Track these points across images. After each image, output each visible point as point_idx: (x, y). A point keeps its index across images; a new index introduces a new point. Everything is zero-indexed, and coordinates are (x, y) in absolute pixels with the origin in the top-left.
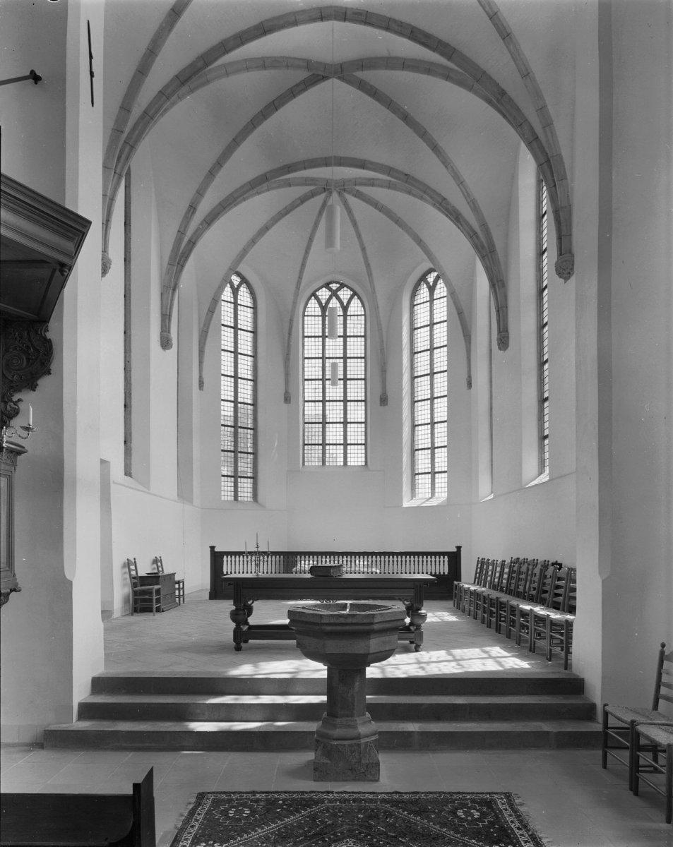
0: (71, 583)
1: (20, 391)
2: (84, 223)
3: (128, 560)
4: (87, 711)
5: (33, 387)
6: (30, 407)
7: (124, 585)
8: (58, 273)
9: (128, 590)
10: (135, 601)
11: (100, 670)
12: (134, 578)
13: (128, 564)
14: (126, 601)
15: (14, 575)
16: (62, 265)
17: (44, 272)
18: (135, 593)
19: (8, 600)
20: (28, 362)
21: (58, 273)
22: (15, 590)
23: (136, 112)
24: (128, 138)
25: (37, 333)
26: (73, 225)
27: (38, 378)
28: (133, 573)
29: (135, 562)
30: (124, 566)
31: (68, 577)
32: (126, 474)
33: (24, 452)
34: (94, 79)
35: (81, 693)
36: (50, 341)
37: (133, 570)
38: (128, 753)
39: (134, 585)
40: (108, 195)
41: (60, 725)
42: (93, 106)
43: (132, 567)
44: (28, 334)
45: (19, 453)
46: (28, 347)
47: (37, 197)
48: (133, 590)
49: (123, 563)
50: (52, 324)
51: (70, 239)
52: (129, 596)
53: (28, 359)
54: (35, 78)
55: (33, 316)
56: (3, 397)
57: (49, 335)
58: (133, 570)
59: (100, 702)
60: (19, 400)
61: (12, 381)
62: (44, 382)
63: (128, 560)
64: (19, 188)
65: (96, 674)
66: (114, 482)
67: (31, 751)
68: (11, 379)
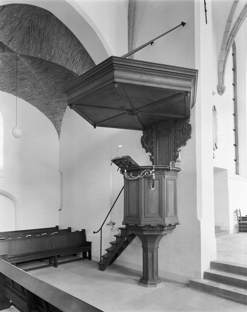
0: (200, 222)
1: (180, 147)
2: (195, 72)
3: (236, 210)
4: (207, 276)
5: (185, 144)
6: (183, 152)
7: (235, 220)
8: (186, 96)
9: (237, 222)
10: (240, 227)
11: (215, 259)
12: (239, 217)
13: (236, 212)
14: (236, 227)
15: (177, 218)
16: (187, 92)
17: (182, 97)
18: (240, 224)
19: (175, 227)
20: (183, 135)
21: (186, 96)
22: (177, 224)
23: (234, 20)
24: (231, 33)
25: (186, 123)
26: (187, 74)
27: (186, 141)
28: (239, 215)
29: (240, 211)
30: (235, 212)
31: (199, 219)
32: (236, 174)
33: (180, 171)
34: (207, 12)
35: (205, 267)
36: (190, 125)
37: (239, 214)
38: (223, 299)
39: (240, 220)
40: (223, 60)
41: (196, 279)
42: (207, 24)
43: (239, 213)
44: (183, 124)
45: (178, 171)
46: (183, 129)
47: (188, 70)
48: (239, 223)
49: (234, 211)
50: (191, 118)
51: (190, 80)
52: (237, 225)
53: (183, 134)
54: (183, 24)
55: (184, 117)
56: (174, 150)
57: (190, 123)
58: (239, 214)
59: (213, 273)
60: (180, 150)
61: (177, 144)
62: (189, 142)
63: (236, 210)
64: (182, 69)
65: (212, 260)
66: (229, 178)
67: (184, 287)
68: (177, 143)
